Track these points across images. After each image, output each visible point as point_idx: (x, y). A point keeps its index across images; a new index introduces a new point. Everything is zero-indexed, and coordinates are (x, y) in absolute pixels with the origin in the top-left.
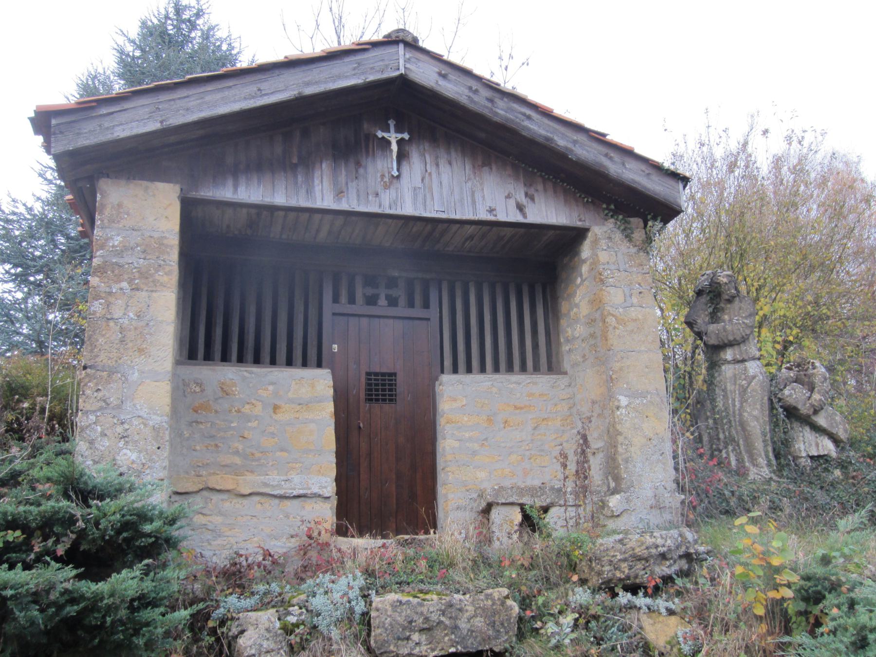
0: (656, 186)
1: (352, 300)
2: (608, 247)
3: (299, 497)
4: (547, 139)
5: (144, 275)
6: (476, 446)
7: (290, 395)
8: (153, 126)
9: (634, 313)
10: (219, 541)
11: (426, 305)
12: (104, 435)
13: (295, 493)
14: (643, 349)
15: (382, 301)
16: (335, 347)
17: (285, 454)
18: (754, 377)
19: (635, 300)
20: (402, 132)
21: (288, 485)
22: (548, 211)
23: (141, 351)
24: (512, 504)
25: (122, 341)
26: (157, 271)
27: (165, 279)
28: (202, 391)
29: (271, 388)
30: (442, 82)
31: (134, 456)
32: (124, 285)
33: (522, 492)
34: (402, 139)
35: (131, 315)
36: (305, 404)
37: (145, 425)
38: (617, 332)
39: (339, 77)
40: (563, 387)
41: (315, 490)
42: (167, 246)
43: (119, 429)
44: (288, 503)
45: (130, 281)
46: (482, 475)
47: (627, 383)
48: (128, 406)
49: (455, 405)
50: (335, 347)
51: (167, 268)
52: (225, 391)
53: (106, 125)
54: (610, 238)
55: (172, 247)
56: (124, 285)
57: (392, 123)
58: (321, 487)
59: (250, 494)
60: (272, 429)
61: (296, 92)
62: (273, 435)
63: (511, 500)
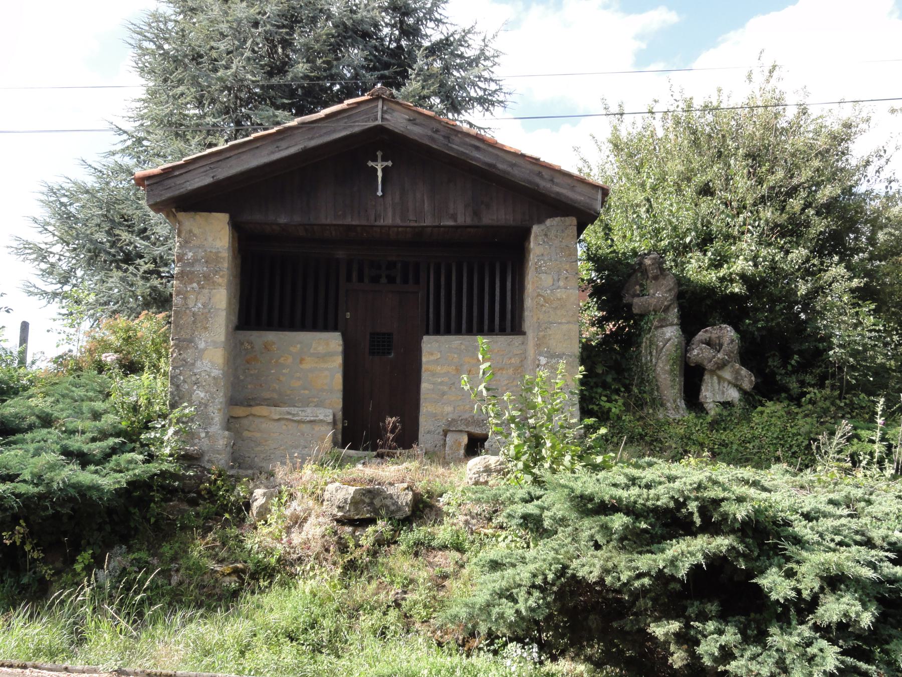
0: (578, 196)
1: (361, 279)
2: (544, 242)
3: (311, 422)
4: (490, 165)
5: (206, 277)
6: (445, 388)
7: (312, 351)
8: (208, 180)
9: (560, 293)
10: (259, 449)
11: (417, 282)
12: (184, 381)
13: (308, 419)
14: (563, 321)
15: (384, 280)
16: (348, 315)
17: (307, 392)
18: (669, 340)
19: (561, 283)
20: (387, 161)
21: (303, 414)
22: (499, 215)
23: (206, 328)
24: (461, 431)
25: (194, 322)
26: (215, 275)
27: (220, 280)
28: (252, 348)
29: (299, 346)
30: (411, 127)
31: (202, 395)
32: (195, 285)
33: (467, 423)
34: (387, 166)
35: (200, 305)
36: (324, 357)
37: (209, 376)
38: (544, 309)
39: (334, 131)
40: (517, 344)
41: (321, 417)
42: (221, 258)
43: (194, 378)
44: (303, 427)
45: (199, 284)
46: (449, 409)
47: (548, 348)
48: (198, 363)
49: (432, 358)
50: (348, 315)
51: (221, 273)
52: (267, 347)
53: (178, 182)
54: (546, 235)
55: (223, 258)
56: (195, 285)
57: (379, 154)
58: (326, 416)
59: (279, 420)
60: (298, 375)
61: (302, 146)
62: (299, 379)
63: (460, 428)
